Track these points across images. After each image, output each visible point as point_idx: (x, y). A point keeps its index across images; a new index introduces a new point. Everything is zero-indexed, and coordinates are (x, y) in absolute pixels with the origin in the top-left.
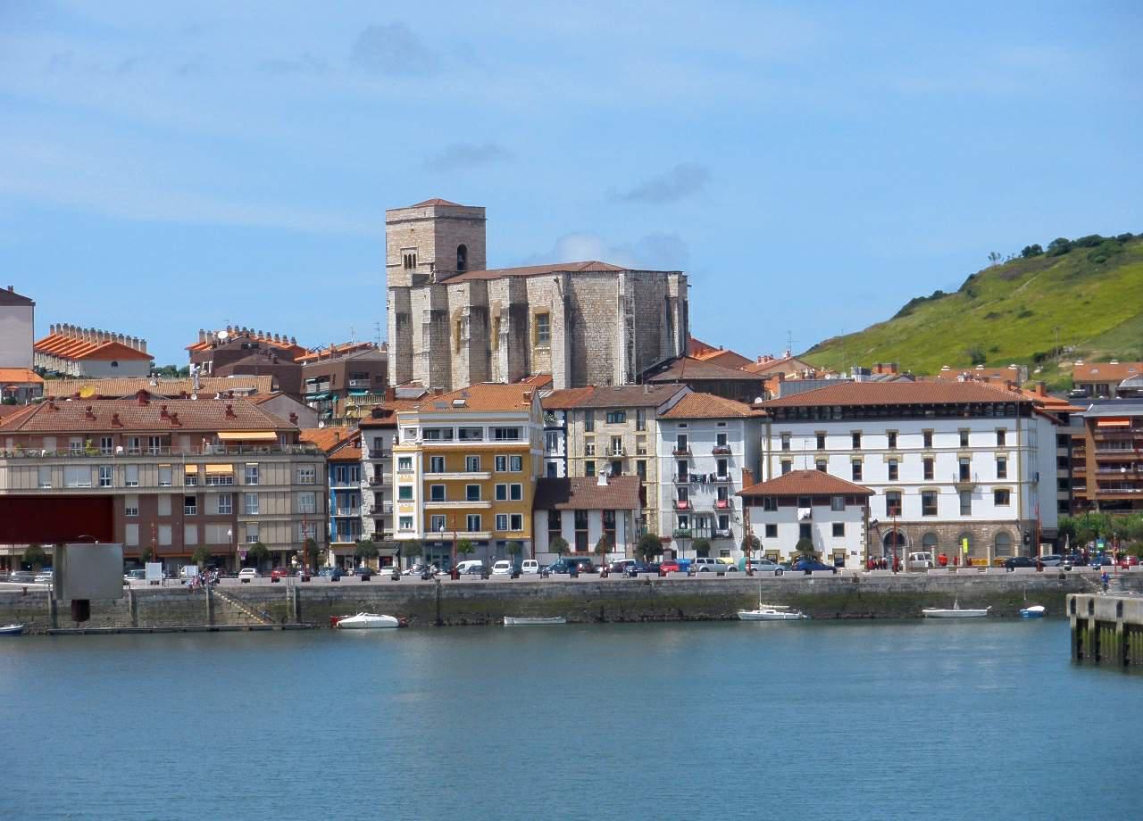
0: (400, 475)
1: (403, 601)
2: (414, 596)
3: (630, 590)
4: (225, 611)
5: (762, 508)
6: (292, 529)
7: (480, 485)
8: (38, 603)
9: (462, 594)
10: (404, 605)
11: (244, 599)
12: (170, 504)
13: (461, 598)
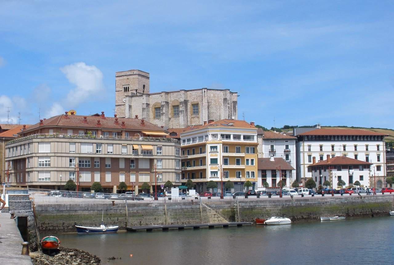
0: (211, 154)
1: (280, 208)
2: (283, 205)
3: (356, 201)
4: (208, 214)
5: (336, 170)
6: (101, 175)
7: (228, 158)
8: (120, 210)
9: (301, 204)
10: (280, 210)
11: (213, 207)
12: (124, 162)
13: (301, 206)
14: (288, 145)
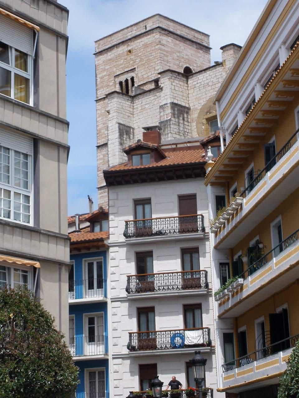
14: (193, 197)
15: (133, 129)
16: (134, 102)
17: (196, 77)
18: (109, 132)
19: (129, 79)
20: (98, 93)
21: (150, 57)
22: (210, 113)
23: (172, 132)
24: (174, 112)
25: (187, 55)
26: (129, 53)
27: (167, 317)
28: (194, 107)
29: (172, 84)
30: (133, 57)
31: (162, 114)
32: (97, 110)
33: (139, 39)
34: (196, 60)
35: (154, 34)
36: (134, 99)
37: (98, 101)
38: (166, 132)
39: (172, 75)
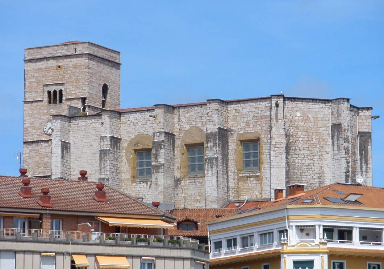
15: (70, 144)
16: (71, 122)
17: (128, 115)
18: (52, 146)
19: (58, 90)
20: (26, 96)
21: (79, 77)
22: (138, 146)
23: (110, 159)
24: (112, 144)
25: (105, 74)
26: (58, 68)
27: (20, 255)
28: (124, 138)
29: (111, 121)
30: (62, 73)
31: (102, 144)
32: (24, 110)
33: (69, 59)
34: (110, 77)
35: (83, 59)
36: (71, 120)
37: (26, 103)
38: (105, 159)
39: (111, 114)
